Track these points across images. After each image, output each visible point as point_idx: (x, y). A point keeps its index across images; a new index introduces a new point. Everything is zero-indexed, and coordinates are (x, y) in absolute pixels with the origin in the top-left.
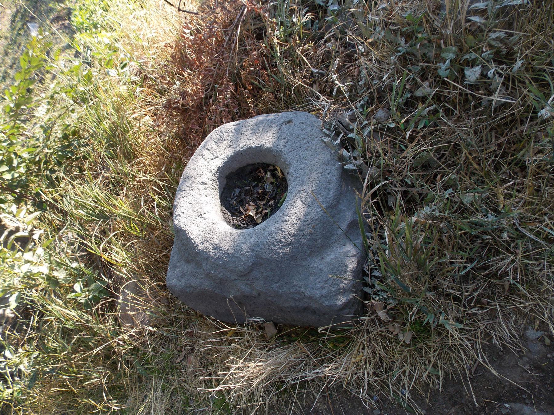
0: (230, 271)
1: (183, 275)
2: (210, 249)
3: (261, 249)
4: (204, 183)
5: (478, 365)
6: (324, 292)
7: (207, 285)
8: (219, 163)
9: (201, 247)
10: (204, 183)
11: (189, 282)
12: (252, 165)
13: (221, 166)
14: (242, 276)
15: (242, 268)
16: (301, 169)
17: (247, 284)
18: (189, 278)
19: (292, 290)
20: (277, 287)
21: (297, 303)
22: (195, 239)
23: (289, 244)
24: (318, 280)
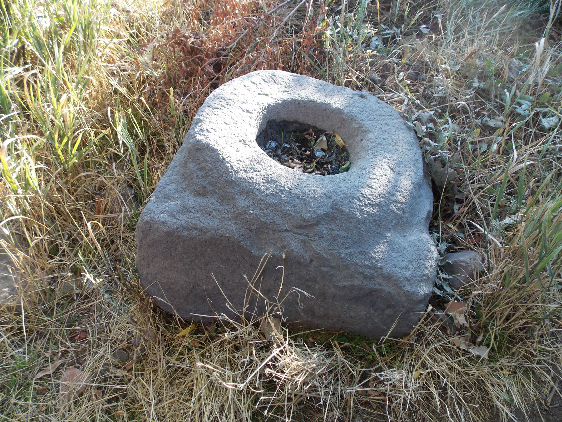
0: (286, 216)
1: (185, 209)
3: (342, 198)
4: (248, 111)
5: (555, 395)
6: (408, 274)
7: (232, 229)
8: (271, 101)
9: (243, 175)
10: (248, 111)
11: (194, 221)
14: (300, 227)
15: (306, 215)
17: (304, 242)
18: (197, 215)
20: (346, 254)
21: (365, 282)
22: (233, 164)
23: (376, 205)
24: (401, 259)
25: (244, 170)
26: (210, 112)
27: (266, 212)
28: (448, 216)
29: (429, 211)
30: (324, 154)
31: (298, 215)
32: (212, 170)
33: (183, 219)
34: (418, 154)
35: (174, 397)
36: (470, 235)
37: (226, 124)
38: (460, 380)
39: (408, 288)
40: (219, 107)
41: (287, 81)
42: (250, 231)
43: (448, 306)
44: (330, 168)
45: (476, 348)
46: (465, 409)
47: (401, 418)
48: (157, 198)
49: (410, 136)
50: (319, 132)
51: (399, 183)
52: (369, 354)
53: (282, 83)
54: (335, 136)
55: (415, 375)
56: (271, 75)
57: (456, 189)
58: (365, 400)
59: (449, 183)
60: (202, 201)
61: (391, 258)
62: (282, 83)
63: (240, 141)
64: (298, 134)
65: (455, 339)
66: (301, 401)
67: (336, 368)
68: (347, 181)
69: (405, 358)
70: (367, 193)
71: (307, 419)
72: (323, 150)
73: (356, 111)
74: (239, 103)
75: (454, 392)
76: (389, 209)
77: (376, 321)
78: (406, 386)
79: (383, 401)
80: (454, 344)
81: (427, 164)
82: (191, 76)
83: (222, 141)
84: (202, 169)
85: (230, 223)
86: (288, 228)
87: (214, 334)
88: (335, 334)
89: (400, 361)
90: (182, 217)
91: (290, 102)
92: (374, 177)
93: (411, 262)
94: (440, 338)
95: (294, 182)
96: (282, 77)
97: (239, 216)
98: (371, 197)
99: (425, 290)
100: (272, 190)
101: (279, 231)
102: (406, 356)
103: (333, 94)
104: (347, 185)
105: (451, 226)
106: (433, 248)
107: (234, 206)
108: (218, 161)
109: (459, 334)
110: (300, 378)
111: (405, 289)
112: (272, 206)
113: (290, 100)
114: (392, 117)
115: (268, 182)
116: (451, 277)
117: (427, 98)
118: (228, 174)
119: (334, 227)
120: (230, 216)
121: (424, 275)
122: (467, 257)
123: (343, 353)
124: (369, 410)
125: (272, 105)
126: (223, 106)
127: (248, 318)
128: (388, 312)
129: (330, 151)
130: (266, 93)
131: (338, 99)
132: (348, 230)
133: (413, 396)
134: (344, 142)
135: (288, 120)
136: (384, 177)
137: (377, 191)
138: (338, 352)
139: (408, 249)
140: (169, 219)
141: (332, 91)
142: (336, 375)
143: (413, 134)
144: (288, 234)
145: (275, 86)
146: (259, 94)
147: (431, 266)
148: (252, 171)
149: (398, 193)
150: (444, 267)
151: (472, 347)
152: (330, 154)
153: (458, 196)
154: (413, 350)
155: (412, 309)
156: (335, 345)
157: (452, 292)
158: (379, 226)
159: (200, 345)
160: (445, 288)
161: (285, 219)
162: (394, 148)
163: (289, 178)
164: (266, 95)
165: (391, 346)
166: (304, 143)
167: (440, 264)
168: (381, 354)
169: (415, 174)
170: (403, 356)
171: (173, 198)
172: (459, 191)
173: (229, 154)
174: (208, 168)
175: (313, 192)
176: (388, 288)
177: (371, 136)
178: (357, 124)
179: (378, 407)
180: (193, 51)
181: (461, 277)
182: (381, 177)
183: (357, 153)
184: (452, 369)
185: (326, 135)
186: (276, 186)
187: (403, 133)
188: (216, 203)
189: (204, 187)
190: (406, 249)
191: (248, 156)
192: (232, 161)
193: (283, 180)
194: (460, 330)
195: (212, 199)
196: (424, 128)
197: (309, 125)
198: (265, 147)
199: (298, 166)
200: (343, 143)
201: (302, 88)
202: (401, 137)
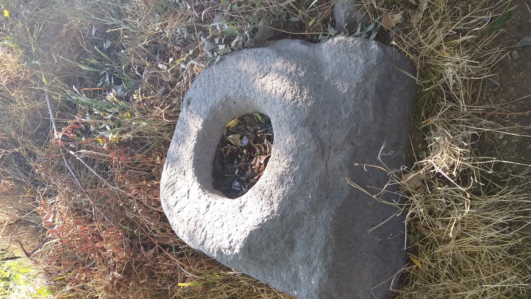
0: (313, 166)
1: (307, 260)
2: (280, 191)
3: (296, 118)
4: (208, 207)
6: (361, 61)
7: (326, 215)
8: (196, 186)
9: (276, 206)
10: (208, 207)
11: (319, 251)
12: (215, 160)
13: (199, 185)
14: (323, 153)
15: (313, 148)
16: (234, 82)
17: (336, 150)
19: (353, 97)
20: (346, 114)
22: (265, 216)
23: (301, 88)
24: (348, 67)
25: (270, 205)
26: (211, 242)
27: (310, 184)
28: (301, 26)
29: (301, 43)
30: (245, 137)
31: (312, 156)
32: (269, 236)
33: (317, 262)
34: (247, 53)
35: (478, 271)
36: (319, 8)
37: (223, 225)
38: (449, 18)
39: (374, 61)
40: (204, 233)
41: (174, 172)
42: (327, 198)
43: (386, 27)
44: (261, 131)
45: (421, 5)
46: (472, 15)
47: (484, 67)
48: (296, 289)
49: (230, 59)
50: (224, 141)
51: (279, 69)
52: (431, 95)
53: (175, 176)
54: (228, 128)
55: (447, 55)
56: (167, 188)
57: (277, 19)
58: (470, 98)
59: (272, 25)
60: (299, 243)
61: (348, 75)
62: (175, 176)
63: (241, 211)
64: (225, 161)
65: (414, 22)
66: (475, 153)
67: (445, 123)
68: (279, 114)
69: (433, 64)
70: (290, 96)
71: (490, 149)
72: (241, 138)
73: (205, 107)
74: (199, 216)
75: (459, 25)
76: (304, 77)
77: (401, 88)
78: (458, 63)
79: (470, 83)
80: (419, 23)
81: (255, 44)
82: (153, 274)
83: (242, 228)
84: (268, 246)
85: (320, 217)
86: (324, 164)
87: (418, 236)
88: (414, 125)
89: (436, 68)
90: (315, 263)
91: (196, 168)
92: (274, 91)
93: (350, 59)
94: (414, 34)
95: (282, 160)
96: (168, 177)
97: (314, 208)
98: (294, 93)
99: (374, 46)
100: (291, 179)
101: (327, 173)
102: (431, 63)
103: (187, 129)
104: (283, 114)
105: (311, 23)
106: (336, 39)
107: (304, 213)
108: (262, 230)
109: (410, 18)
110: (458, 151)
111: (375, 64)
112: (305, 179)
113: (194, 169)
114: (211, 75)
115: (282, 183)
116: (360, 25)
117: (186, 44)
118: (275, 220)
119: (322, 125)
120: (314, 217)
121: (362, 48)
122: (341, 11)
123: (431, 117)
124: (479, 95)
125: (199, 185)
126: (203, 230)
127: (404, 200)
128: (394, 78)
129: (243, 131)
130: (186, 192)
131: (192, 124)
132: (324, 112)
133: (465, 57)
134: (234, 119)
135: (212, 171)
136: (274, 82)
137: (288, 88)
138: (432, 121)
139: (338, 61)
140: (316, 275)
141: (183, 130)
142: (451, 123)
143: (227, 57)
144: (329, 165)
145: (179, 184)
146: (188, 198)
147: (353, 41)
148: (271, 198)
149: (289, 70)
150: (351, 31)
151: (421, 9)
152: (246, 131)
153: (284, 17)
154: (425, 57)
155: (392, 58)
156: (424, 124)
157: (373, 24)
158: (319, 86)
159: (429, 248)
160: (369, 30)
161: (315, 167)
162: (243, 73)
163: (278, 164)
164: (189, 191)
165: (423, 76)
166: (235, 155)
167: (348, 34)
168: (431, 83)
169: (268, 55)
170: (431, 65)
171: (296, 272)
172: (279, 17)
173: (255, 220)
174: (263, 242)
175: (291, 143)
176: (375, 77)
177: (231, 93)
178: (218, 106)
179: (476, 87)
180: (127, 273)
181: (359, 16)
182: (274, 85)
183: (247, 106)
184: (440, 25)
185: (227, 135)
186: (286, 175)
187: (227, 65)
188: (301, 231)
189: (286, 243)
190: (338, 63)
191: (257, 202)
192: (262, 216)
193: (280, 170)
194: (406, 17)
195: (297, 235)
196: (221, 47)
197: (216, 151)
198: (239, 191)
199: (259, 160)
200: (235, 120)
201: (181, 158)
202: (232, 67)
